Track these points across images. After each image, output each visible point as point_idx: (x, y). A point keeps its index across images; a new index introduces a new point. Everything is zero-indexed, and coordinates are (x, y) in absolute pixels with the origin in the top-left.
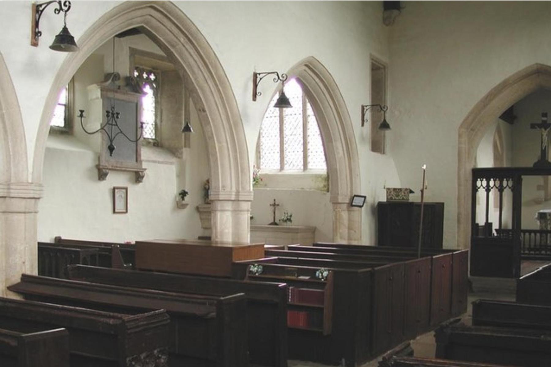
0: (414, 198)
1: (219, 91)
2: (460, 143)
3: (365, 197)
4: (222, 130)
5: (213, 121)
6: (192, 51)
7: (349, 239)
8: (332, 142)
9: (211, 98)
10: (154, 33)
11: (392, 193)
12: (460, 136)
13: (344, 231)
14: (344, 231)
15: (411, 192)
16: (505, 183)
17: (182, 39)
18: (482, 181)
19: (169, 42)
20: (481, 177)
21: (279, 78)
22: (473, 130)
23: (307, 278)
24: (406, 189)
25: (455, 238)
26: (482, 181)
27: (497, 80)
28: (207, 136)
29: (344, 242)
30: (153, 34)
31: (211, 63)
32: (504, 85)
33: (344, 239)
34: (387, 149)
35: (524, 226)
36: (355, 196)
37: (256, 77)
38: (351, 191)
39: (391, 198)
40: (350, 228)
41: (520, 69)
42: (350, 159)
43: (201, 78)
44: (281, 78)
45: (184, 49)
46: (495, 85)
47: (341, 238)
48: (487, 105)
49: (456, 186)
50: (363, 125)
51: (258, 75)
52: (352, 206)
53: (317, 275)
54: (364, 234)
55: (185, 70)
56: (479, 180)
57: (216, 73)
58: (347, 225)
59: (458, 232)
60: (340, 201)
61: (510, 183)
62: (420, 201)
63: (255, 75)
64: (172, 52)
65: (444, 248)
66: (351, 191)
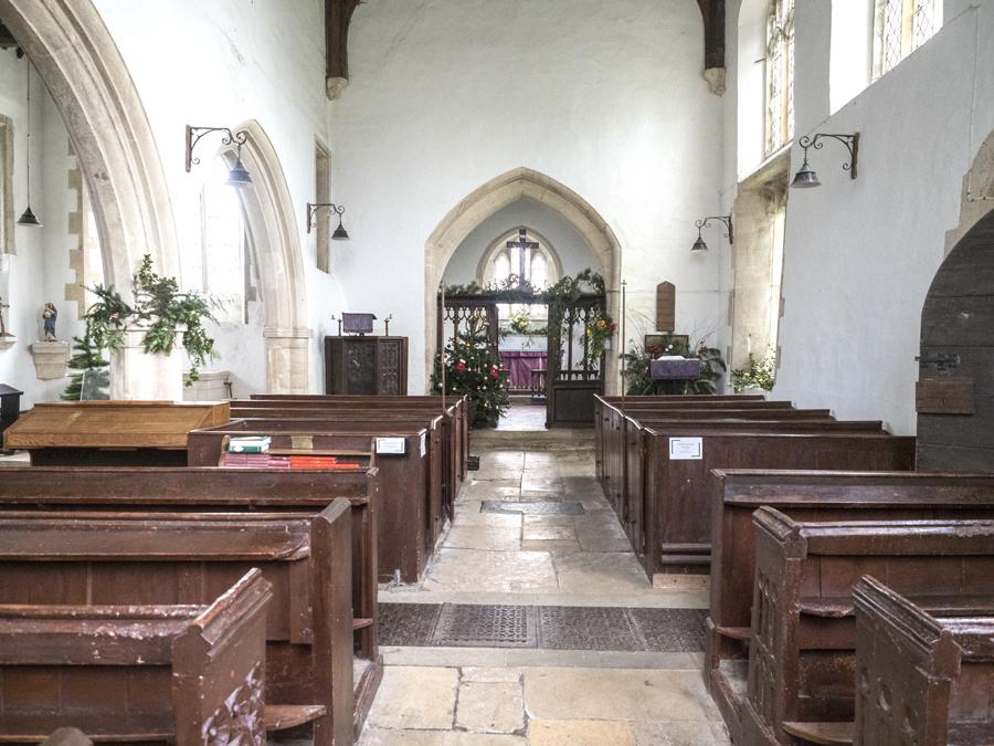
1: (134, 145)
2: (427, 261)
4: (137, 213)
5: (122, 197)
6: (91, 64)
7: (293, 387)
8: (270, 252)
9: (119, 155)
10: (18, 9)
12: (427, 253)
13: (285, 376)
14: (285, 376)
16: (461, 313)
17: (74, 37)
19: (48, 37)
21: (232, 138)
22: (440, 246)
28: (108, 222)
30: (18, 13)
31: (123, 94)
32: (483, 191)
34: (331, 268)
37: (191, 134)
40: (292, 372)
41: (502, 172)
43: (103, 118)
44: (235, 139)
45: (75, 56)
46: (471, 192)
50: (309, 232)
51: (193, 131)
55: (74, 99)
57: (130, 113)
58: (288, 368)
60: (280, 335)
62: (337, 334)
63: (190, 130)
64: (51, 58)
65: (409, 394)
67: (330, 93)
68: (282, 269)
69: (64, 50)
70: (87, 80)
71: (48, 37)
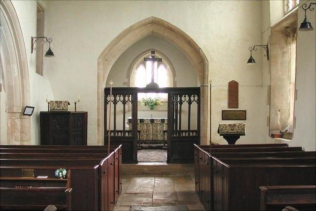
0: (71, 109)
2: (99, 69)
3: (33, 108)
7: (22, 140)
11: (54, 105)
12: (99, 64)
15: (69, 104)
18: (120, 97)
20: (120, 94)
22: (106, 60)
23: (46, 177)
24: (66, 102)
25: (95, 137)
26: (120, 97)
27: (126, 26)
29: (18, 144)
32: (130, 30)
33: (18, 141)
34: (44, 72)
35: (191, 129)
36: (26, 107)
38: (23, 103)
39: (54, 109)
40: (22, 132)
42: (22, 77)
47: (16, 140)
48: (118, 43)
49: (96, 100)
50: (32, 52)
52: (24, 114)
53: (57, 174)
54: (32, 138)
56: (118, 96)
59: (98, 133)
60: (15, 111)
61: (196, 98)
65: (88, 145)
66: (23, 103)
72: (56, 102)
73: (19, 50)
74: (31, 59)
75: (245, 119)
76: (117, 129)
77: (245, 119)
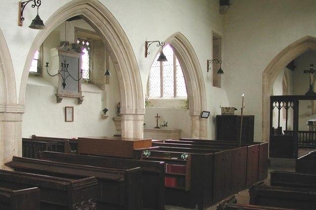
0: (237, 113)
2: (263, 81)
3: (209, 112)
6: (110, 29)
12: (263, 77)
13: (197, 132)
14: (197, 132)
15: (236, 109)
17: (105, 22)
18: (276, 103)
19: (97, 24)
20: (276, 101)
24: (233, 108)
25: (260, 136)
26: (276, 103)
27: (284, 46)
29: (197, 138)
32: (289, 48)
35: (300, 129)
40: (200, 130)
43: (115, 44)
49: (262, 106)
50: (208, 71)
52: (202, 117)
54: (209, 134)
57: (124, 42)
60: (195, 114)
63: (146, 43)
67: (222, 12)
68: (195, 87)
69: (102, 27)
70: (110, 34)
71: (97, 24)
72: (226, 108)
73: (196, 70)
74: (207, 77)
75: (254, 116)
76: (300, 129)
77: (254, 116)
